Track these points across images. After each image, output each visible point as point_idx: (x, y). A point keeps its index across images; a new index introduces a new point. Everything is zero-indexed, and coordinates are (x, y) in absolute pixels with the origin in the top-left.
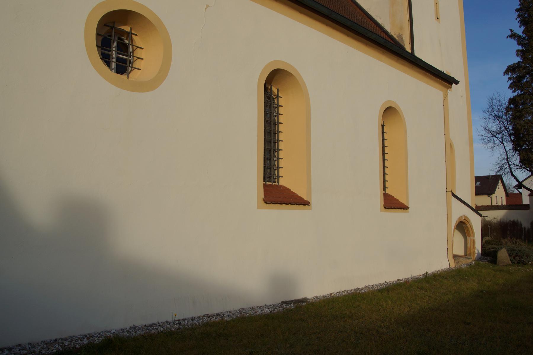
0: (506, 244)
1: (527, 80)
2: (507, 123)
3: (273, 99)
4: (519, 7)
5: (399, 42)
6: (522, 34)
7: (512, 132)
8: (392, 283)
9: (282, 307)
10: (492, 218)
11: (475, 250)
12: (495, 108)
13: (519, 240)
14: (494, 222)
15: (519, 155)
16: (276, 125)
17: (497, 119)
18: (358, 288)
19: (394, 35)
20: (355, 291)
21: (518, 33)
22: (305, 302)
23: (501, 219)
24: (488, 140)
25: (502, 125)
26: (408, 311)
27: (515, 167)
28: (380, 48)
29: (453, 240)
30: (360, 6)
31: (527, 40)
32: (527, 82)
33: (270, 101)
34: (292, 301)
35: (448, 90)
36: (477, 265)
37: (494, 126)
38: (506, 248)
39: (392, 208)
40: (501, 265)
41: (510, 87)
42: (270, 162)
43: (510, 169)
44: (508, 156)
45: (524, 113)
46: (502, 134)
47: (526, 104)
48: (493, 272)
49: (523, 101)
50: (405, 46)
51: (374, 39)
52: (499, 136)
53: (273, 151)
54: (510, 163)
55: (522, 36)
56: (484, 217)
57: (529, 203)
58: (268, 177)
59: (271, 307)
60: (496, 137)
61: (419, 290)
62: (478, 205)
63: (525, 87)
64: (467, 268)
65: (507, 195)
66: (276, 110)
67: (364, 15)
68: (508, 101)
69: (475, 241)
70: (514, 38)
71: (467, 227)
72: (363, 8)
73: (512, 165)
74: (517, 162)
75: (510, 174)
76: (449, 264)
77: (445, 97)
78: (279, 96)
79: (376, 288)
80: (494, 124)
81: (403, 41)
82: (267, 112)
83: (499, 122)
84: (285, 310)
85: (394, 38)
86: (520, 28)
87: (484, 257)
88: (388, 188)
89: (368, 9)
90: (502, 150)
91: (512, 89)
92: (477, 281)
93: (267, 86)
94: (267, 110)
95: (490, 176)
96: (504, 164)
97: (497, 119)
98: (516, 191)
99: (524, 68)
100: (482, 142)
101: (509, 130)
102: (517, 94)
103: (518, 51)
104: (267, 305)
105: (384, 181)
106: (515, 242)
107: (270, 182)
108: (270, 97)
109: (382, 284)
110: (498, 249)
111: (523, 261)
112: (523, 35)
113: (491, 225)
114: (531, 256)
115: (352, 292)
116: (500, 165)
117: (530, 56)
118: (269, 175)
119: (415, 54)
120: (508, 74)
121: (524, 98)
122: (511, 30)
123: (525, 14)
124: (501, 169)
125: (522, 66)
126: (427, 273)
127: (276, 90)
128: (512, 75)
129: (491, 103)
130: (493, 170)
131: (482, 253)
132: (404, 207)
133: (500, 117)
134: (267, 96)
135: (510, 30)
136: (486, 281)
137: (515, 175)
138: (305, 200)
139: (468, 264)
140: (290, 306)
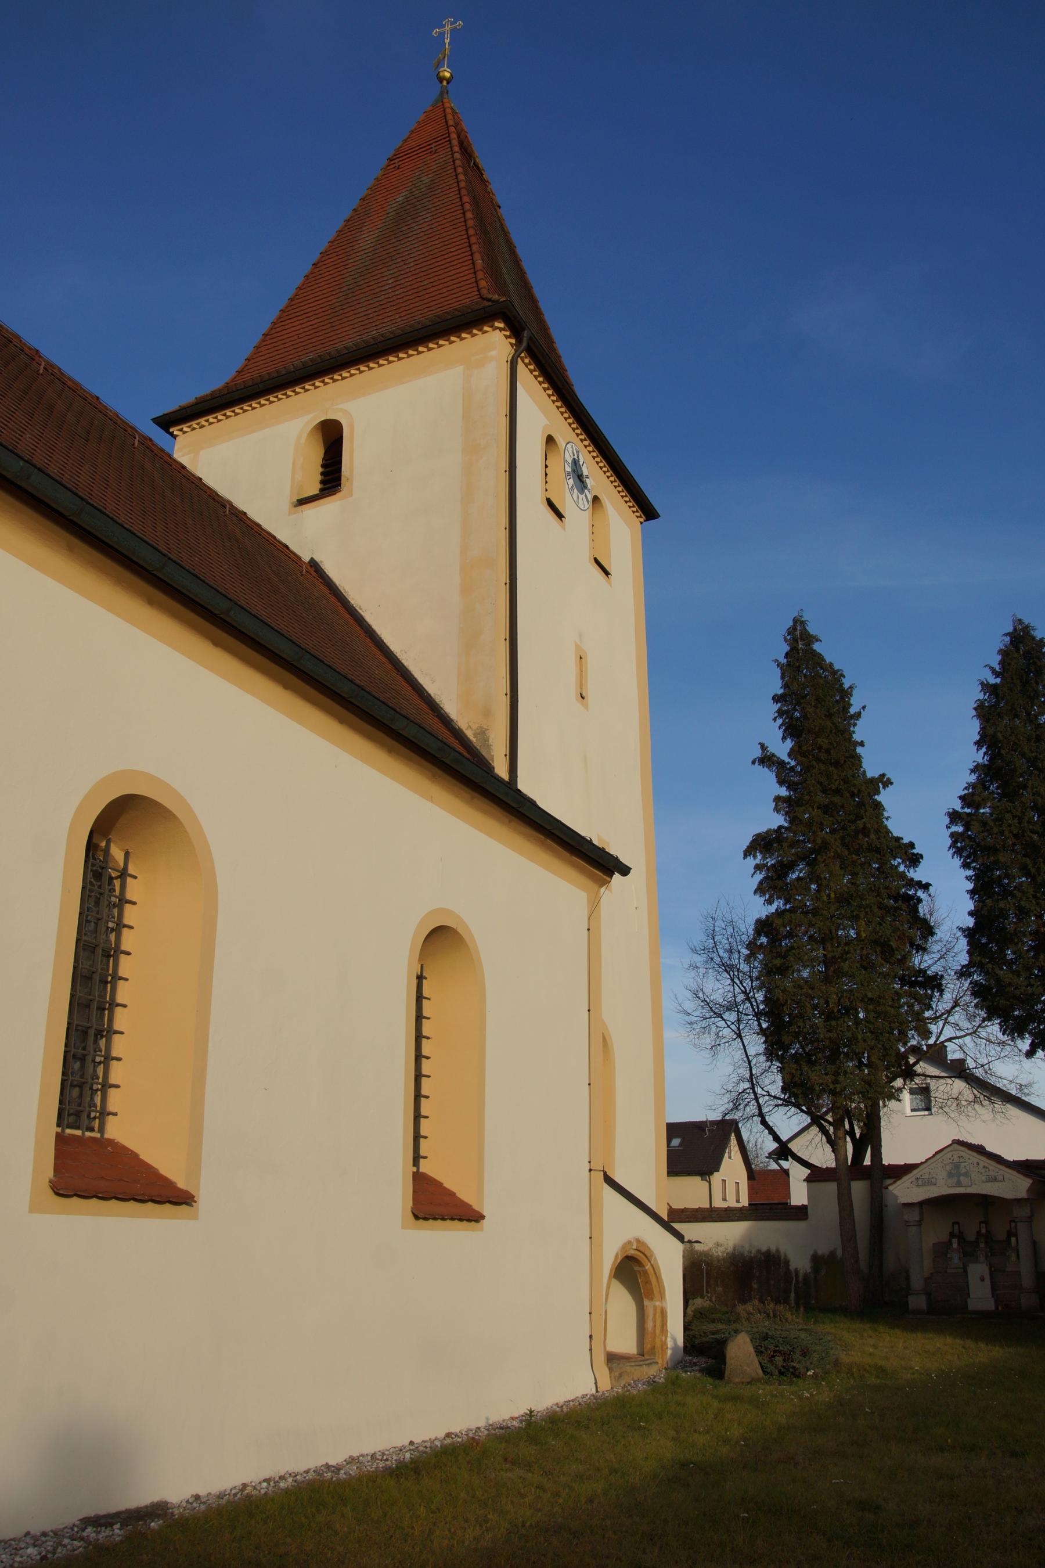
0: (748, 1320)
1: (801, 875)
2: (752, 983)
3: (111, 879)
4: (780, 691)
5: (477, 749)
6: (787, 759)
7: (763, 1009)
8: (428, 1445)
9: (82, 1539)
10: (711, 1245)
11: (666, 1339)
12: (720, 942)
13: (780, 1307)
14: (716, 1254)
15: (781, 1070)
16: (109, 956)
17: (727, 972)
18: (327, 1464)
19: (467, 729)
20: (319, 1474)
21: (778, 754)
22: (158, 1516)
23: (734, 1248)
24: (703, 1026)
25: (740, 988)
26: (475, 1538)
27: (771, 1102)
28: (426, 764)
29: (606, 1311)
30: (383, 641)
31: (800, 774)
32: (799, 879)
33: (99, 883)
34: (117, 1515)
35: (603, 889)
36: (673, 1382)
37: (719, 989)
38: (747, 1332)
39: (435, 1219)
40: (737, 1380)
41: (760, 890)
42: (82, 1067)
43: (759, 1107)
44: (754, 1072)
45: (791, 959)
46: (738, 1011)
47: (797, 936)
48: (716, 1404)
49: (791, 929)
50: (493, 761)
51: (412, 739)
52: (731, 1017)
53: (96, 1035)
54: (759, 1091)
55: (789, 763)
56: (690, 1242)
57: (806, 1203)
58: (72, 1111)
59: (46, 1541)
60: (722, 1018)
61: (507, 1466)
62: (674, 1206)
63: (796, 893)
64: (645, 1392)
65: (751, 1175)
66: (115, 911)
67: (390, 666)
68: (753, 927)
69: (666, 1313)
70: (769, 767)
71: (646, 1272)
72: (388, 647)
73: (764, 1096)
74: (776, 1089)
75: (758, 1119)
76: (596, 1383)
77: (594, 907)
78: (129, 872)
79: (381, 1464)
80: (718, 985)
81: (488, 747)
82: (87, 916)
83: (732, 980)
84: (91, 1547)
85: (466, 736)
86: (783, 742)
87: (690, 1358)
88: (425, 1157)
89: (401, 651)
90: (739, 1054)
91: (764, 895)
92: (673, 1433)
93: (95, 840)
94: (88, 910)
95: (706, 1122)
96: (743, 1092)
97: (726, 971)
98: (774, 1166)
99: (794, 844)
100: (688, 1030)
101: (756, 1002)
102: (777, 910)
103: (778, 799)
104: (32, 1532)
105: (417, 1137)
106: (772, 1315)
107: (78, 1128)
108: (101, 874)
109: (401, 1450)
110: (727, 1335)
111: (794, 1367)
112: (790, 760)
113: (708, 1264)
114: (815, 1351)
115: (310, 1480)
116: (734, 1095)
117: (807, 816)
118: (74, 1107)
119: (520, 786)
120: (755, 857)
121: (794, 921)
122: (763, 747)
123: (795, 710)
124: (736, 1107)
125: (787, 838)
126: (531, 1411)
127: (123, 854)
128: (764, 858)
129: (712, 928)
130: (714, 1108)
131: (685, 1347)
132: (471, 1216)
133: (733, 965)
134: (92, 870)
135: (759, 746)
136: (695, 1431)
137: (771, 1124)
138: (181, 1190)
139: (648, 1382)
140: (108, 1532)
